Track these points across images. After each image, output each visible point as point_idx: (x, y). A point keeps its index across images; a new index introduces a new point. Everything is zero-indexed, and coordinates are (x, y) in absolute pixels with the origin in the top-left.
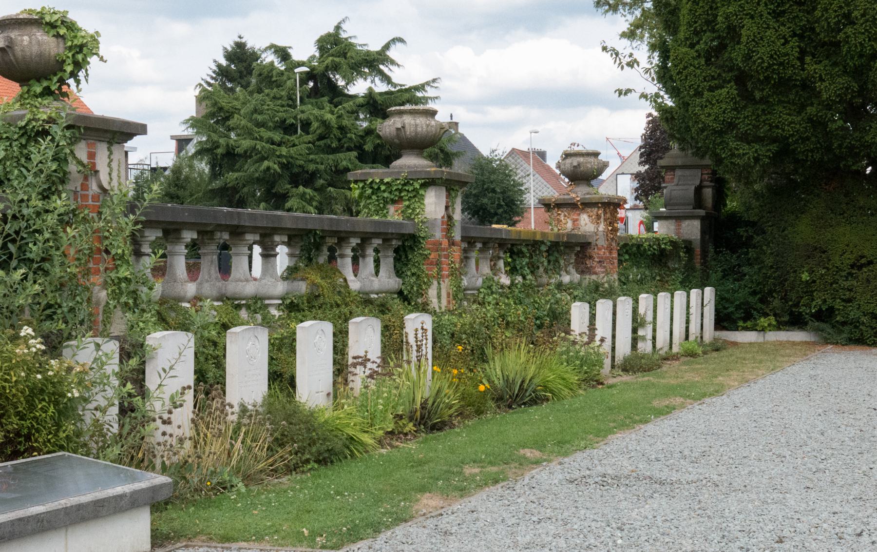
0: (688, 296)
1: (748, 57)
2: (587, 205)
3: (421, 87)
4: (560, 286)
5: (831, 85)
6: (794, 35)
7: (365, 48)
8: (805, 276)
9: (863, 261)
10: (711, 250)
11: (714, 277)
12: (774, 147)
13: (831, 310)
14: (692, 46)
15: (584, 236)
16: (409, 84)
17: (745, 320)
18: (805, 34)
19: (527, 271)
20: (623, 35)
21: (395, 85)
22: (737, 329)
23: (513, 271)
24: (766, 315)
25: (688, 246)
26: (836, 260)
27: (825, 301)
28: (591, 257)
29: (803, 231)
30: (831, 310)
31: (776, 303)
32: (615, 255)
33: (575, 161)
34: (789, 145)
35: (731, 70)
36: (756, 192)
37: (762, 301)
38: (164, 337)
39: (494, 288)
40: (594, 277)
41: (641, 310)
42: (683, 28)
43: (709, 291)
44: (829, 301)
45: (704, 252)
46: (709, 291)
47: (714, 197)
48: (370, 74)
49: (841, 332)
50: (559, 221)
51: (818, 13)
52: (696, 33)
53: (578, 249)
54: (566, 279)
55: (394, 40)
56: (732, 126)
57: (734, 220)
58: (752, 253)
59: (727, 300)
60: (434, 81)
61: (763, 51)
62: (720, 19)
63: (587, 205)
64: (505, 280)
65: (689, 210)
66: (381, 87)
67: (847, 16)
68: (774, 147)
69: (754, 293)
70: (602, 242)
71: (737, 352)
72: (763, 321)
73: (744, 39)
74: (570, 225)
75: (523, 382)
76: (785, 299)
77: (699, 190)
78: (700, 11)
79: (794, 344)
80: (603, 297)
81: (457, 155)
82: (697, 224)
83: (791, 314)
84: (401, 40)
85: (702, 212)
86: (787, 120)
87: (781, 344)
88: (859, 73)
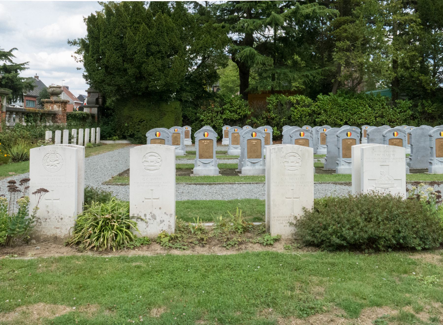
0: (96, 129)
1: (108, 62)
2: (56, 102)
3: (23, 64)
4: (45, 127)
5: (131, 71)
6: (121, 56)
7: (3, 50)
8: (126, 125)
9: (142, 120)
10: (100, 117)
11: (101, 124)
12: (116, 87)
13: (134, 134)
14: (92, 57)
15: (54, 112)
16: (18, 63)
17: (109, 137)
18: (124, 56)
19: (32, 121)
20: (76, 53)
21: (13, 63)
22: (107, 140)
23: (27, 121)
24: (115, 136)
25: (93, 116)
26: (135, 120)
27: (132, 132)
28: (57, 118)
29: (126, 112)
30: (134, 134)
31: (118, 132)
32: (65, 117)
33: (53, 89)
34: (120, 87)
35: (103, 65)
36: (113, 100)
37: (115, 132)
38: (373, 149)
39: (20, 126)
40: (58, 124)
41: (72, 134)
42: (90, 52)
43: (98, 129)
44: (133, 132)
45: (98, 117)
46: (98, 129)
47: (102, 101)
48: (5, 59)
49: (136, 141)
50: (47, 107)
51: (127, 50)
52: (93, 53)
53: (53, 116)
54: (48, 124)
55: (14, 49)
56: (104, 81)
57: (108, 108)
58: (112, 118)
59: (104, 131)
60: (28, 62)
61: (112, 60)
62: (100, 50)
63: (56, 102)
64: (24, 124)
65: (94, 105)
66: (8, 63)
67: (135, 52)
68: (116, 87)
69: (112, 129)
70: (60, 113)
71: (104, 146)
72: (114, 138)
73: (107, 56)
74: (51, 108)
75: (22, 154)
76: (121, 131)
77: (97, 99)
78: (95, 47)
79: (123, 144)
80: (59, 129)
81: (35, 86)
82: (96, 109)
83: (123, 135)
84: (16, 49)
85: (98, 106)
86: (119, 80)
87: (119, 144)
88: (139, 67)
